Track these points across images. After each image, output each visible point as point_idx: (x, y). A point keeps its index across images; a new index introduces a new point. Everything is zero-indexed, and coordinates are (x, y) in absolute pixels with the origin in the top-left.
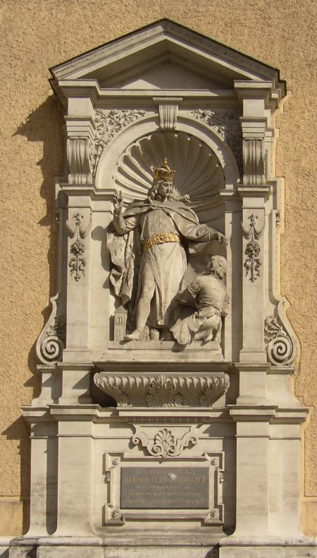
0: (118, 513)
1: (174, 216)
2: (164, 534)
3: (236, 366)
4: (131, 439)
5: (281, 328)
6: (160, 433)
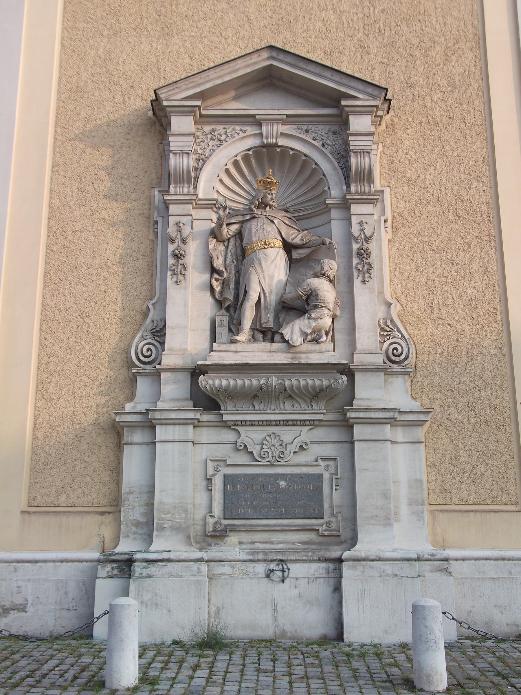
0: (220, 524)
1: (278, 223)
2: (272, 546)
3: (351, 367)
4: (236, 443)
5: (395, 330)
6: (268, 438)
